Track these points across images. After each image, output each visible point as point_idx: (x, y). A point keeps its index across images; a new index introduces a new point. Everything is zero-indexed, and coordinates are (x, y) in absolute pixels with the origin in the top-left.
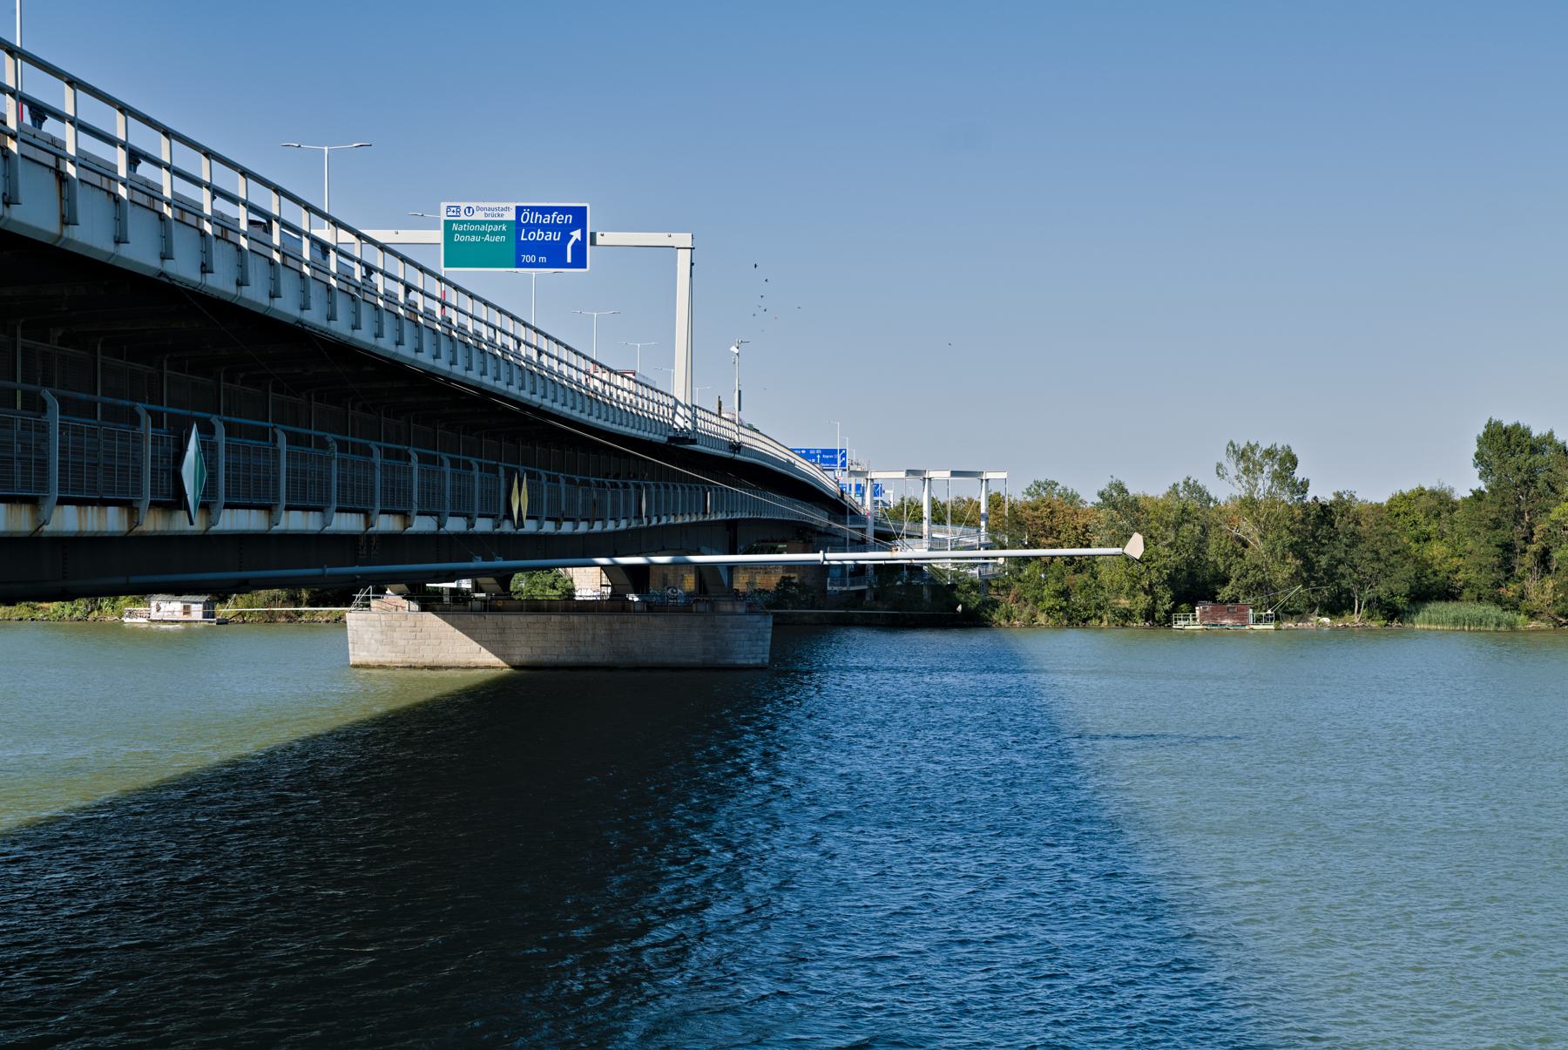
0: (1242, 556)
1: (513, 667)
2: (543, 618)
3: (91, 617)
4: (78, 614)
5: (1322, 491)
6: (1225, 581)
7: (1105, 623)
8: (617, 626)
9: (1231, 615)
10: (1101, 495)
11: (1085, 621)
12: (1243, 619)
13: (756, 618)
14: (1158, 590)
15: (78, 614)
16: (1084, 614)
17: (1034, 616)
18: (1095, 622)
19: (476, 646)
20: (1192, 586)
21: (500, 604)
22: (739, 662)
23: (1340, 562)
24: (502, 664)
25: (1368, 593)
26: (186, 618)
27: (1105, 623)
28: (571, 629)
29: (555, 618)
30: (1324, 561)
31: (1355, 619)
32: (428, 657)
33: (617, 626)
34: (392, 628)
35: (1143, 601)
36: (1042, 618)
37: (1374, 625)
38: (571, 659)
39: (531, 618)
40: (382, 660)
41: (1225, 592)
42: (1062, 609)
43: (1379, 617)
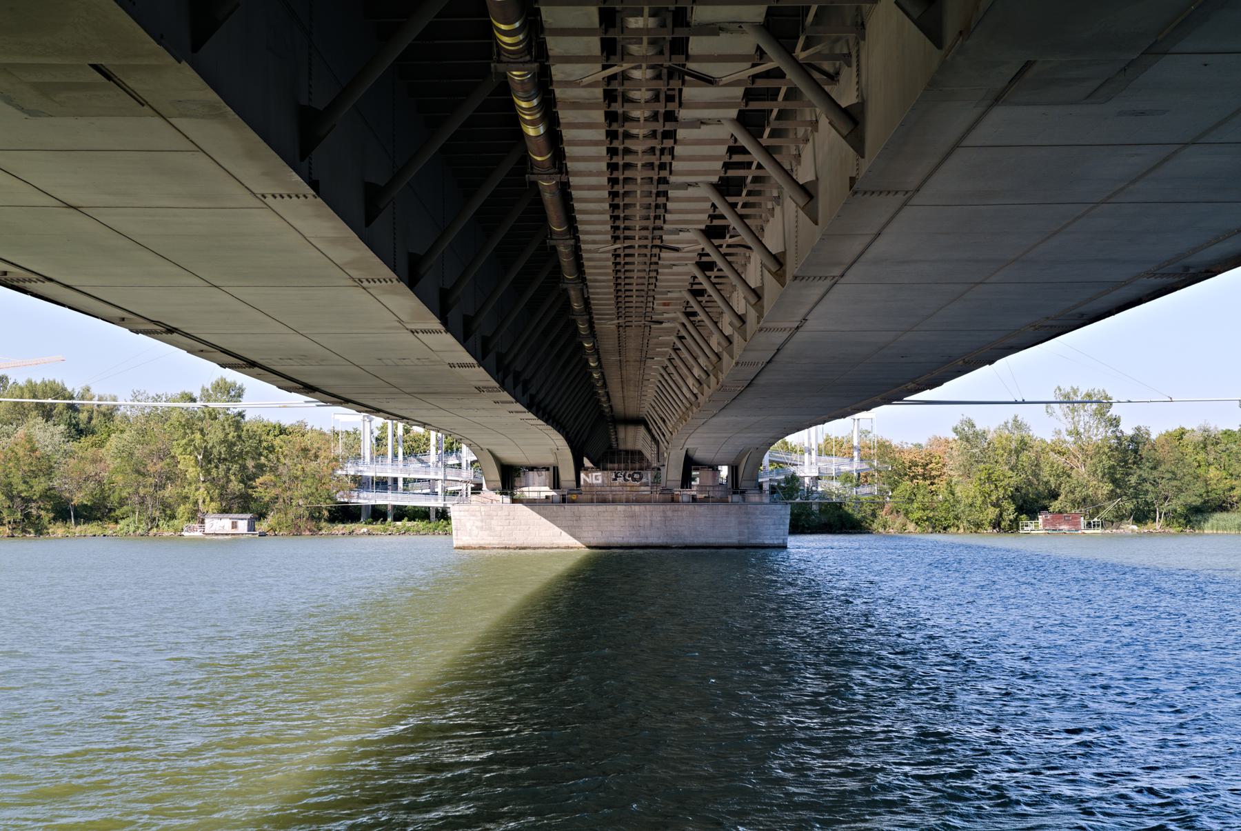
0: (1069, 476)
1: (589, 547)
2: (610, 508)
3: (151, 533)
4: (140, 531)
5: (1127, 429)
6: (1054, 495)
7: (962, 530)
8: (669, 513)
9: (1067, 522)
10: (955, 430)
11: (945, 529)
12: (1076, 525)
13: (779, 507)
14: (1005, 504)
15: (140, 531)
16: (945, 523)
17: (905, 525)
18: (953, 530)
19: (558, 530)
20: (1029, 504)
21: (574, 497)
22: (766, 542)
23: (1145, 480)
24: (579, 544)
25: (1166, 507)
26: (234, 531)
27: (962, 530)
28: (633, 516)
29: (620, 508)
30: (1133, 480)
31: (1157, 526)
32: (520, 540)
33: (669, 513)
34: (490, 517)
35: (992, 513)
36: (911, 527)
37: (1172, 531)
38: (634, 541)
39: (602, 508)
40: (482, 543)
41: (1056, 505)
42: (928, 519)
43: (1176, 524)
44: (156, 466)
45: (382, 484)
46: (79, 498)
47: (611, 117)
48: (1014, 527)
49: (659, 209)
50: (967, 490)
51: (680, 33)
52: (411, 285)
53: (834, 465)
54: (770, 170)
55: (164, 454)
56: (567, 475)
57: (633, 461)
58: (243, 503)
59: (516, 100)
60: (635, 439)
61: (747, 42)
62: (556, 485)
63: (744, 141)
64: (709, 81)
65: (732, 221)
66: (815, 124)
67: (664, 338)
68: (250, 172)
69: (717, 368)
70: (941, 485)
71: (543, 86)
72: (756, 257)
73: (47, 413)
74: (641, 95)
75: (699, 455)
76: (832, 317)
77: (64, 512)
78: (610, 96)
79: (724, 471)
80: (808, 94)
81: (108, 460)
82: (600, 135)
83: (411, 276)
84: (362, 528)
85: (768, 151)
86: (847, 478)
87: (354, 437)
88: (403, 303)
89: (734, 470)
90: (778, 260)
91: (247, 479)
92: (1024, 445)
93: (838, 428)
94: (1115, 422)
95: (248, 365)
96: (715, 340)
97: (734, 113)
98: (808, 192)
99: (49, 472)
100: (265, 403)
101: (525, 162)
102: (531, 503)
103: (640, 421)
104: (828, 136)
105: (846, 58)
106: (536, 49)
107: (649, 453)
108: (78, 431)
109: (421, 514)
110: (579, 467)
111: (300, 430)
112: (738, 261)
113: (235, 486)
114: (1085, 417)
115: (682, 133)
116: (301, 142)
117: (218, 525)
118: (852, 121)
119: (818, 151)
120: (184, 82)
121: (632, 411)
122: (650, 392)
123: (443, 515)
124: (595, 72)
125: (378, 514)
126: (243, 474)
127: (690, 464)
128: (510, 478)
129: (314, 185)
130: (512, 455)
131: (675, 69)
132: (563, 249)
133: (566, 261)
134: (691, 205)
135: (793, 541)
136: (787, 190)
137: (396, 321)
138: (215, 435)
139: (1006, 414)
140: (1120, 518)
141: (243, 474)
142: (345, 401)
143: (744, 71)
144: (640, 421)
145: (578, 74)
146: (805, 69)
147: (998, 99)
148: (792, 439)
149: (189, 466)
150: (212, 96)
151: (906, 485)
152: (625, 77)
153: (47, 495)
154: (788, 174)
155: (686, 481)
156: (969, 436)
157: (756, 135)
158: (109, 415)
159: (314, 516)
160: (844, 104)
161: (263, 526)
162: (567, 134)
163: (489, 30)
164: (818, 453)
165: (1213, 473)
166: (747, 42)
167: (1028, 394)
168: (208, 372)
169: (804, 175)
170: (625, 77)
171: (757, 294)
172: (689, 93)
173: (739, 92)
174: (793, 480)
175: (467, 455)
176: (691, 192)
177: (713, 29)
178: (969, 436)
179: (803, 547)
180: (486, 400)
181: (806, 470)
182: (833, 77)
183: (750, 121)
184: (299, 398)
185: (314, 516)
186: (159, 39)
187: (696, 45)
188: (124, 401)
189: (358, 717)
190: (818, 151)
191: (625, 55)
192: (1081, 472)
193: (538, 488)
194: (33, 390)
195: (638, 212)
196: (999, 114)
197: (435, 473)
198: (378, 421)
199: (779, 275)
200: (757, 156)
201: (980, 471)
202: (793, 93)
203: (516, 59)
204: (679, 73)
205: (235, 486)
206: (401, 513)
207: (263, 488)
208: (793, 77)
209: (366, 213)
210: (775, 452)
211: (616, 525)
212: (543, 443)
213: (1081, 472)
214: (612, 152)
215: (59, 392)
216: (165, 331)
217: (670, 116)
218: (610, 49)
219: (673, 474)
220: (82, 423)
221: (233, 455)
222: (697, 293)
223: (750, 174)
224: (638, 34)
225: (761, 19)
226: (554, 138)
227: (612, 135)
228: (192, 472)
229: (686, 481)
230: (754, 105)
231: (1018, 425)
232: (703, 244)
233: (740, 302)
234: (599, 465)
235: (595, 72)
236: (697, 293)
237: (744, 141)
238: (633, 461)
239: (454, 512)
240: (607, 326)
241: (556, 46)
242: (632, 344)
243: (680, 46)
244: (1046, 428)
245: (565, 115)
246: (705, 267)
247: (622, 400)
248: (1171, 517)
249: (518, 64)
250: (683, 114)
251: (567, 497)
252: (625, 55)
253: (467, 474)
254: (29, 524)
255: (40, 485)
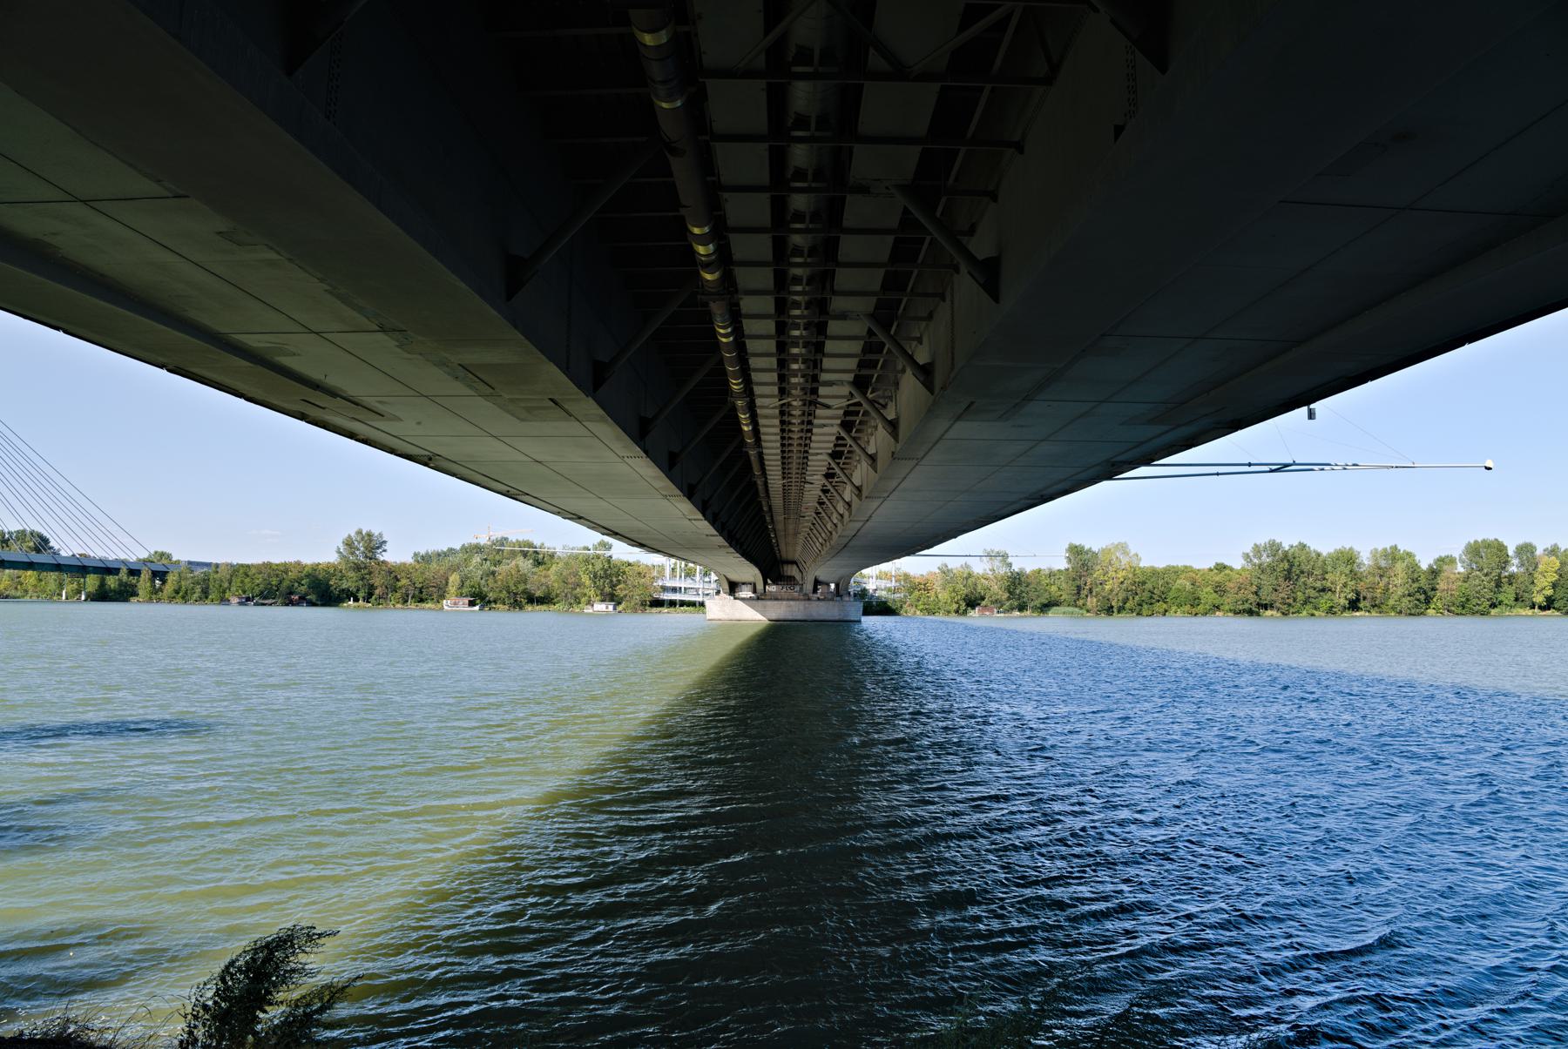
5: (1016, 568)
6: (983, 599)
20: (972, 602)
32: (738, 616)
35: (955, 606)
44: (572, 580)
45: (674, 590)
46: (538, 594)
47: (782, 422)
48: (965, 612)
49: (804, 465)
50: (944, 596)
51: (821, 338)
52: (689, 498)
53: (883, 584)
54: (855, 448)
55: (576, 574)
56: (760, 587)
57: (791, 580)
58: (612, 598)
59: (658, 102)
60: (792, 570)
61: (845, 390)
62: (754, 591)
63: (843, 434)
64: (828, 407)
65: (837, 471)
66: (876, 428)
67: (805, 526)
68: (617, 446)
69: (830, 538)
70: (932, 593)
71: (752, 408)
72: (849, 488)
73: (525, 555)
74: (797, 413)
75: (821, 578)
76: (886, 514)
77: (532, 600)
78: (782, 413)
79: (833, 586)
80: (873, 414)
81: (550, 577)
82: (777, 430)
83: (690, 493)
84: (665, 610)
85: (854, 439)
86: (889, 590)
87: (662, 568)
88: (684, 507)
89: (837, 586)
90: (859, 489)
91: (613, 586)
92: (970, 575)
93: (885, 567)
94: (1010, 565)
95: (614, 534)
96: (829, 526)
97: (850, 377)
98: (873, 459)
99: (525, 582)
100: (622, 552)
101: (743, 442)
102: (743, 599)
103: (794, 562)
104: (910, 384)
105: (890, 398)
106: (749, 392)
107: (798, 577)
108: (538, 563)
109: (692, 604)
110: (765, 583)
111: (638, 564)
112: (840, 489)
113: (607, 590)
114: (997, 563)
115: (815, 430)
116: (640, 433)
117: (600, 607)
118: (893, 426)
119: (878, 440)
120: (590, 406)
121: (790, 557)
122: (799, 548)
123: (702, 604)
124: (776, 402)
125: (672, 603)
126: (611, 584)
127: (817, 582)
128: (733, 587)
129: (646, 452)
130: (734, 577)
131: (812, 400)
132: (760, 482)
133: (761, 488)
134: (819, 461)
135: (864, 619)
136: (863, 457)
137: (682, 514)
138: (598, 566)
139: (962, 561)
140: (1012, 609)
141: (611, 584)
142: (658, 551)
143: (844, 403)
144: (794, 562)
145: (768, 403)
146: (872, 402)
147: (959, 418)
148: (865, 571)
149: (586, 580)
150: (601, 412)
151: (916, 593)
152: (789, 404)
153: (524, 592)
154: (863, 450)
155: (815, 590)
156: (945, 571)
157: (849, 431)
158: (552, 556)
159: (643, 604)
160: (980, 257)
161: (620, 608)
162: (762, 430)
163: (727, 383)
164: (876, 578)
165: (1054, 588)
166: (845, 390)
167: (970, 553)
168: (594, 537)
169: (871, 450)
170: (789, 404)
171: (849, 504)
172: (819, 412)
173: (841, 412)
174: (864, 591)
175: (714, 577)
176: (826, 430)
177: (830, 384)
178: (945, 571)
179: (869, 622)
180: (723, 551)
181: (871, 586)
182: (884, 406)
183: (847, 426)
184: (637, 550)
185: (643, 604)
186: (579, 387)
187: (822, 391)
188: (559, 550)
189: (643, 708)
190: (878, 440)
191: (789, 394)
192: (995, 588)
193: (746, 593)
194: (520, 544)
195: (794, 466)
196: (959, 425)
197: (701, 584)
198: (673, 560)
199: (859, 496)
200: (849, 441)
201: (949, 588)
202: (866, 413)
203: (739, 396)
204: (814, 403)
205: (607, 590)
206: (683, 603)
207: (620, 591)
208: (866, 406)
209: (669, 464)
210: (857, 577)
211: (780, 610)
212: (748, 572)
213: (995, 588)
214: (783, 438)
215: (531, 545)
216: (578, 518)
217: (810, 423)
218: (783, 392)
219: (809, 587)
220: (540, 559)
221: (607, 575)
222: (821, 504)
223: (846, 450)
224: (795, 386)
225: (871, 309)
226: (756, 432)
227: (783, 431)
228: (588, 582)
229: (815, 590)
230: (865, 372)
231: (967, 566)
232: (824, 481)
233: (841, 508)
234: (775, 582)
235: (776, 402)
236: (821, 504)
237: (843, 434)
238: (791, 580)
239: (707, 603)
240: (779, 518)
241: (757, 390)
242: (791, 527)
243: (814, 391)
244: (980, 567)
245: (761, 421)
246: (825, 491)
247: (786, 551)
248: (1034, 609)
249: (740, 398)
250: (816, 422)
251: (760, 597)
252: (789, 394)
253: (714, 585)
254: (516, 605)
255: (521, 587)
